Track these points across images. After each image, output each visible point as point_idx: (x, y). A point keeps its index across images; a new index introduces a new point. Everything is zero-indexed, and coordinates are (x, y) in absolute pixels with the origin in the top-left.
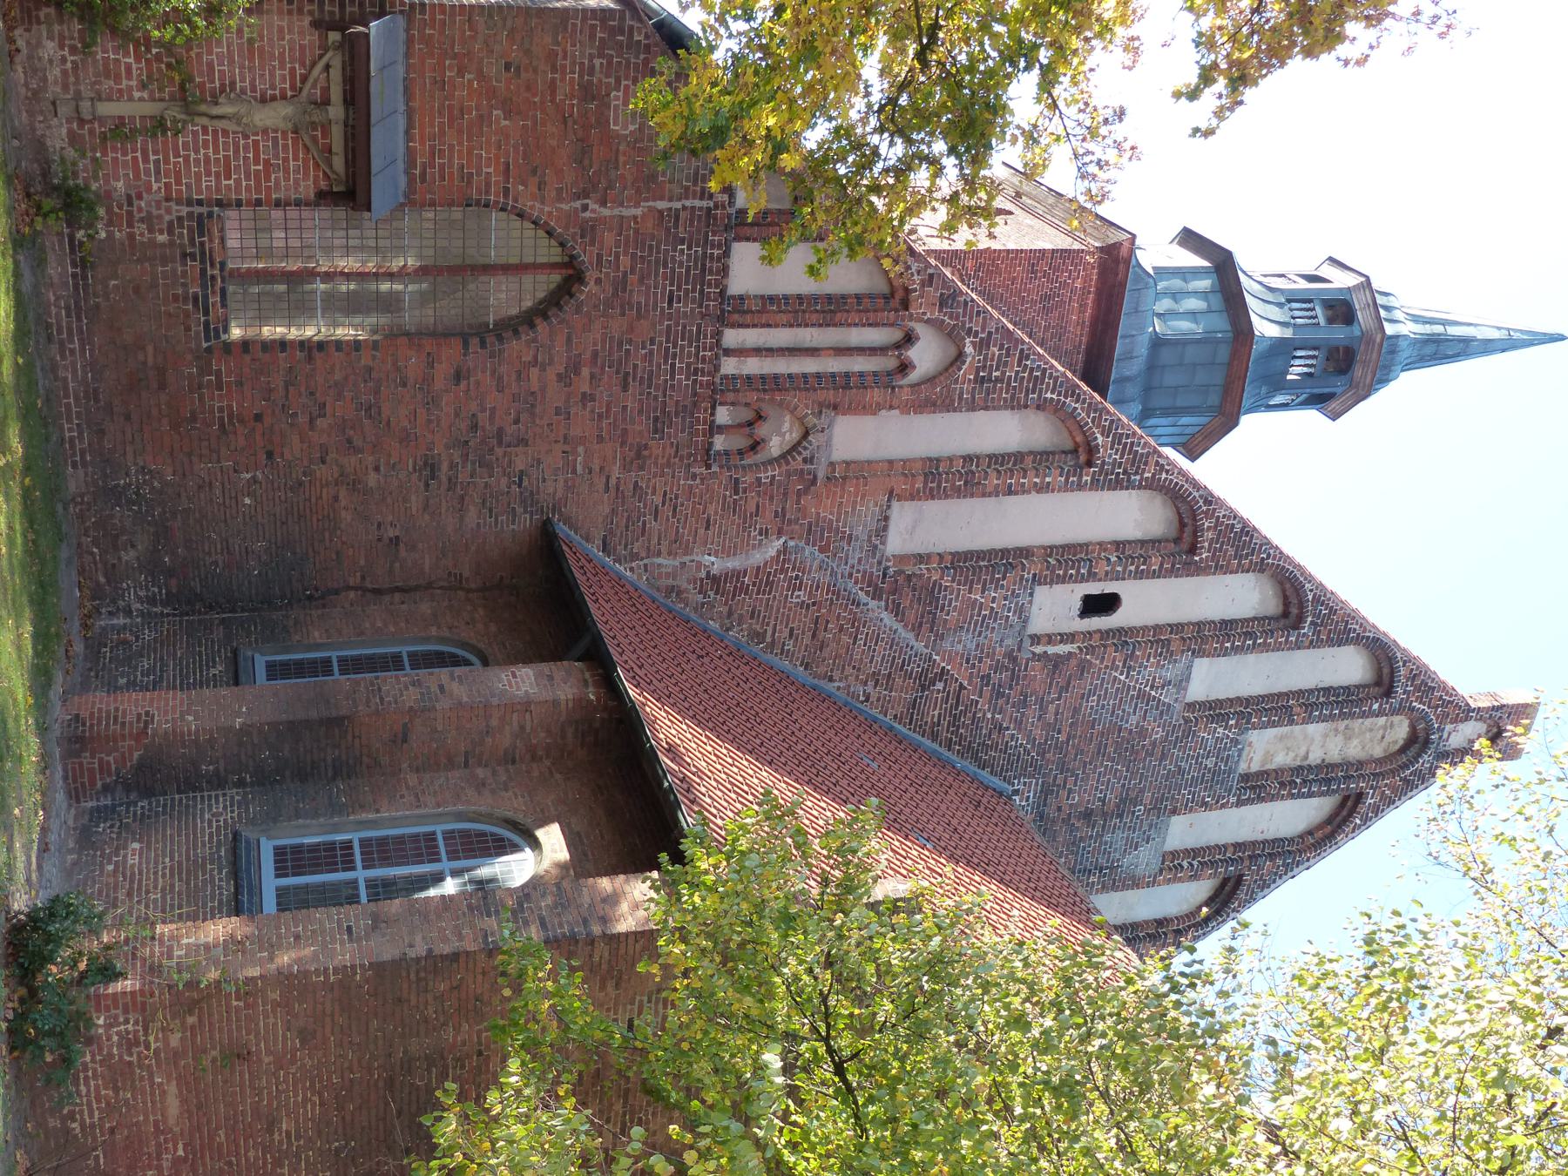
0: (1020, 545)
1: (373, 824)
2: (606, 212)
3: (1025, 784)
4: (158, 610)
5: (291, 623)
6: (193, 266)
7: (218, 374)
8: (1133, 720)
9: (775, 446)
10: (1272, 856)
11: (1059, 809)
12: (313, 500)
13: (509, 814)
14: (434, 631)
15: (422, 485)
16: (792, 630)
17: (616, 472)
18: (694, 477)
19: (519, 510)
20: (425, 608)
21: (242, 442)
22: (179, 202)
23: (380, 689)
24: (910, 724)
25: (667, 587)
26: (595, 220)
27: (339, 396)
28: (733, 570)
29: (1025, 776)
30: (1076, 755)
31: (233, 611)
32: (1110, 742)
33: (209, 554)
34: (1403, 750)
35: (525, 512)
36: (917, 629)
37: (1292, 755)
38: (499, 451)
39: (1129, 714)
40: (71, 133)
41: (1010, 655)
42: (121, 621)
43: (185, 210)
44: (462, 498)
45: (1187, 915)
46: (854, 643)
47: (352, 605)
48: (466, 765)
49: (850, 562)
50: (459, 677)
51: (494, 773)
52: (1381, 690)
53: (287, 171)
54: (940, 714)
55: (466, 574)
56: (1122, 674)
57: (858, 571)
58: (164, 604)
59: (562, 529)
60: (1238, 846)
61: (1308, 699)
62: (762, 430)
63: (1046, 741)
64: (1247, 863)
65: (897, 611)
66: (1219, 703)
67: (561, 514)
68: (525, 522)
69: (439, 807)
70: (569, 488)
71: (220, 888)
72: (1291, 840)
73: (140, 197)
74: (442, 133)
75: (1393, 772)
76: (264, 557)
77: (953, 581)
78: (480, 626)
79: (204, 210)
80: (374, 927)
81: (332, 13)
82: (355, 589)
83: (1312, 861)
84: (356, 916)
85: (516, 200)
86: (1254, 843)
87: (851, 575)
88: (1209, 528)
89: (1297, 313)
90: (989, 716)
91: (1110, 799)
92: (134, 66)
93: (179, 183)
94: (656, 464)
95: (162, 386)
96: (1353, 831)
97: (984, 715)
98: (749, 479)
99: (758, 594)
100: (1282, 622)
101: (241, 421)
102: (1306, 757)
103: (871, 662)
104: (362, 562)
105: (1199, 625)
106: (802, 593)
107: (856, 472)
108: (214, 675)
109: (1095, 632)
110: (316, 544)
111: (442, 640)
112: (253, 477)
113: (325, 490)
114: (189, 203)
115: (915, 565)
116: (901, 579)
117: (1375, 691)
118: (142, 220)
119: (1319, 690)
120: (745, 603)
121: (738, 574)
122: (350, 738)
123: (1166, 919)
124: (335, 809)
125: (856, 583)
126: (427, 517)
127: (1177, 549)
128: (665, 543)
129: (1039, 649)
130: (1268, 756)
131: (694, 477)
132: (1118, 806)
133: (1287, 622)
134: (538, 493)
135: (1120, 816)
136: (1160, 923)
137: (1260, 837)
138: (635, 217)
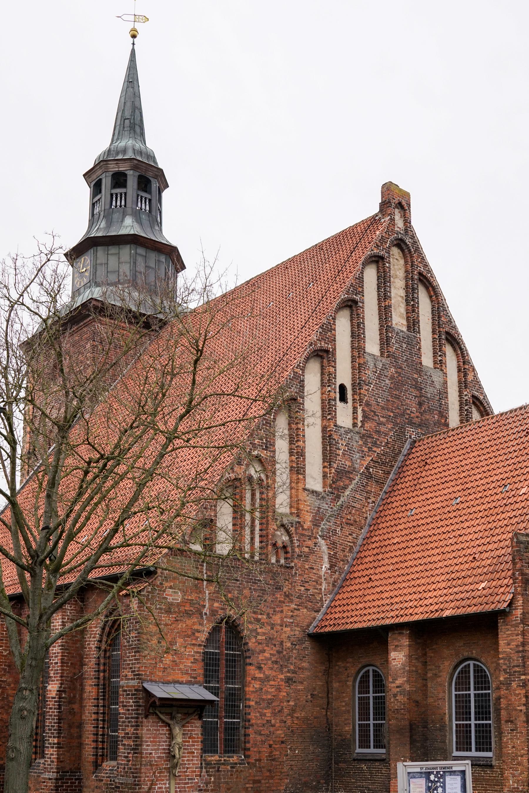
0: (321, 430)
2: (207, 605)
3: (408, 433)
4: (330, 788)
5: (339, 737)
6: (222, 768)
7: (256, 760)
8: (387, 382)
9: (285, 538)
10: (439, 317)
11: (417, 417)
12: (297, 726)
13: (452, 667)
14: (350, 683)
15: (294, 684)
16: (349, 534)
18: (296, 573)
19: (304, 646)
20: (336, 685)
21: (278, 753)
22: (201, 772)
23: (396, 709)
24: (383, 483)
25: (333, 586)
26: (210, 610)
28: (329, 559)
29: (405, 433)
30: (398, 408)
31: (332, 759)
32: (395, 393)
33: (313, 767)
34: (402, 250)
35: (304, 643)
36: (351, 479)
37: (401, 304)
38: (285, 653)
39: (385, 384)
41: (361, 438)
43: (204, 770)
44: (299, 668)
45: (457, 357)
46: (355, 507)
47: (332, 714)
48: (426, 680)
49: (327, 508)
50: (393, 680)
51: (431, 670)
52: (380, 261)
53: (192, 730)
54: (381, 470)
55: (324, 668)
56: (370, 386)
57: (330, 505)
58: (328, 786)
59: (311, 630)
60: (434, 332)
61: (382, 297)
62: (280, 544)
63: (392, 422)
64: (441, 329)
65: (345, 488)
66: (381, 339)
67: (306, 629)
69: (445, 692)
70: (297, 626)
71: (476, 771)
72: (433, 307)
73: (200, 786)
75: (412, 257)
76: (315, 746)
77: (335, 463)
78: (348, 665)
79: (203, 763)
80: (512, 722)
81: (142, 710)
82: (327, 712)
83: (443, 298)
84: (506, 727)
85: (203, 642)
86: (433, 324)
87: (332, 508)
88: (320, 344)
89: (118, 203)
90: (383, 448)
91: (415, 393)
92: (159, 786)
93: (195, 772)
94: (291, 589)
95: (259, 781)
96: (433, 277)
97: (382, 450)
98: (297, 550)
99: (337, 548)
102: (402, 297)
103: (362, 500)
104: (318, 709)
106: (338, 530)
108: (367, 768)
109: (353, 397)
110: (312, 726)
111: (451, 679)
112: (289, 749)
113: (295, 722)
114: (201, 768)
115: (328, 479)
116: (334, 486)
117: (381, 264)
118: (207, 786)
119: (378, 291)
120: (340, 554)
121: (330, 557)
122: (416, 722)
123: (458, 367)
124: (443, 728)
125: (334, 506)
126: (305, 683)
127: (326, 358)
130: (401, 316)
131: (296, 573)
132: (418, 390)
133: (354, 306)
134: (298, 638)
135: (421, 389)
136: (459, 371)
137: (431, 321)
138: (209, 594)
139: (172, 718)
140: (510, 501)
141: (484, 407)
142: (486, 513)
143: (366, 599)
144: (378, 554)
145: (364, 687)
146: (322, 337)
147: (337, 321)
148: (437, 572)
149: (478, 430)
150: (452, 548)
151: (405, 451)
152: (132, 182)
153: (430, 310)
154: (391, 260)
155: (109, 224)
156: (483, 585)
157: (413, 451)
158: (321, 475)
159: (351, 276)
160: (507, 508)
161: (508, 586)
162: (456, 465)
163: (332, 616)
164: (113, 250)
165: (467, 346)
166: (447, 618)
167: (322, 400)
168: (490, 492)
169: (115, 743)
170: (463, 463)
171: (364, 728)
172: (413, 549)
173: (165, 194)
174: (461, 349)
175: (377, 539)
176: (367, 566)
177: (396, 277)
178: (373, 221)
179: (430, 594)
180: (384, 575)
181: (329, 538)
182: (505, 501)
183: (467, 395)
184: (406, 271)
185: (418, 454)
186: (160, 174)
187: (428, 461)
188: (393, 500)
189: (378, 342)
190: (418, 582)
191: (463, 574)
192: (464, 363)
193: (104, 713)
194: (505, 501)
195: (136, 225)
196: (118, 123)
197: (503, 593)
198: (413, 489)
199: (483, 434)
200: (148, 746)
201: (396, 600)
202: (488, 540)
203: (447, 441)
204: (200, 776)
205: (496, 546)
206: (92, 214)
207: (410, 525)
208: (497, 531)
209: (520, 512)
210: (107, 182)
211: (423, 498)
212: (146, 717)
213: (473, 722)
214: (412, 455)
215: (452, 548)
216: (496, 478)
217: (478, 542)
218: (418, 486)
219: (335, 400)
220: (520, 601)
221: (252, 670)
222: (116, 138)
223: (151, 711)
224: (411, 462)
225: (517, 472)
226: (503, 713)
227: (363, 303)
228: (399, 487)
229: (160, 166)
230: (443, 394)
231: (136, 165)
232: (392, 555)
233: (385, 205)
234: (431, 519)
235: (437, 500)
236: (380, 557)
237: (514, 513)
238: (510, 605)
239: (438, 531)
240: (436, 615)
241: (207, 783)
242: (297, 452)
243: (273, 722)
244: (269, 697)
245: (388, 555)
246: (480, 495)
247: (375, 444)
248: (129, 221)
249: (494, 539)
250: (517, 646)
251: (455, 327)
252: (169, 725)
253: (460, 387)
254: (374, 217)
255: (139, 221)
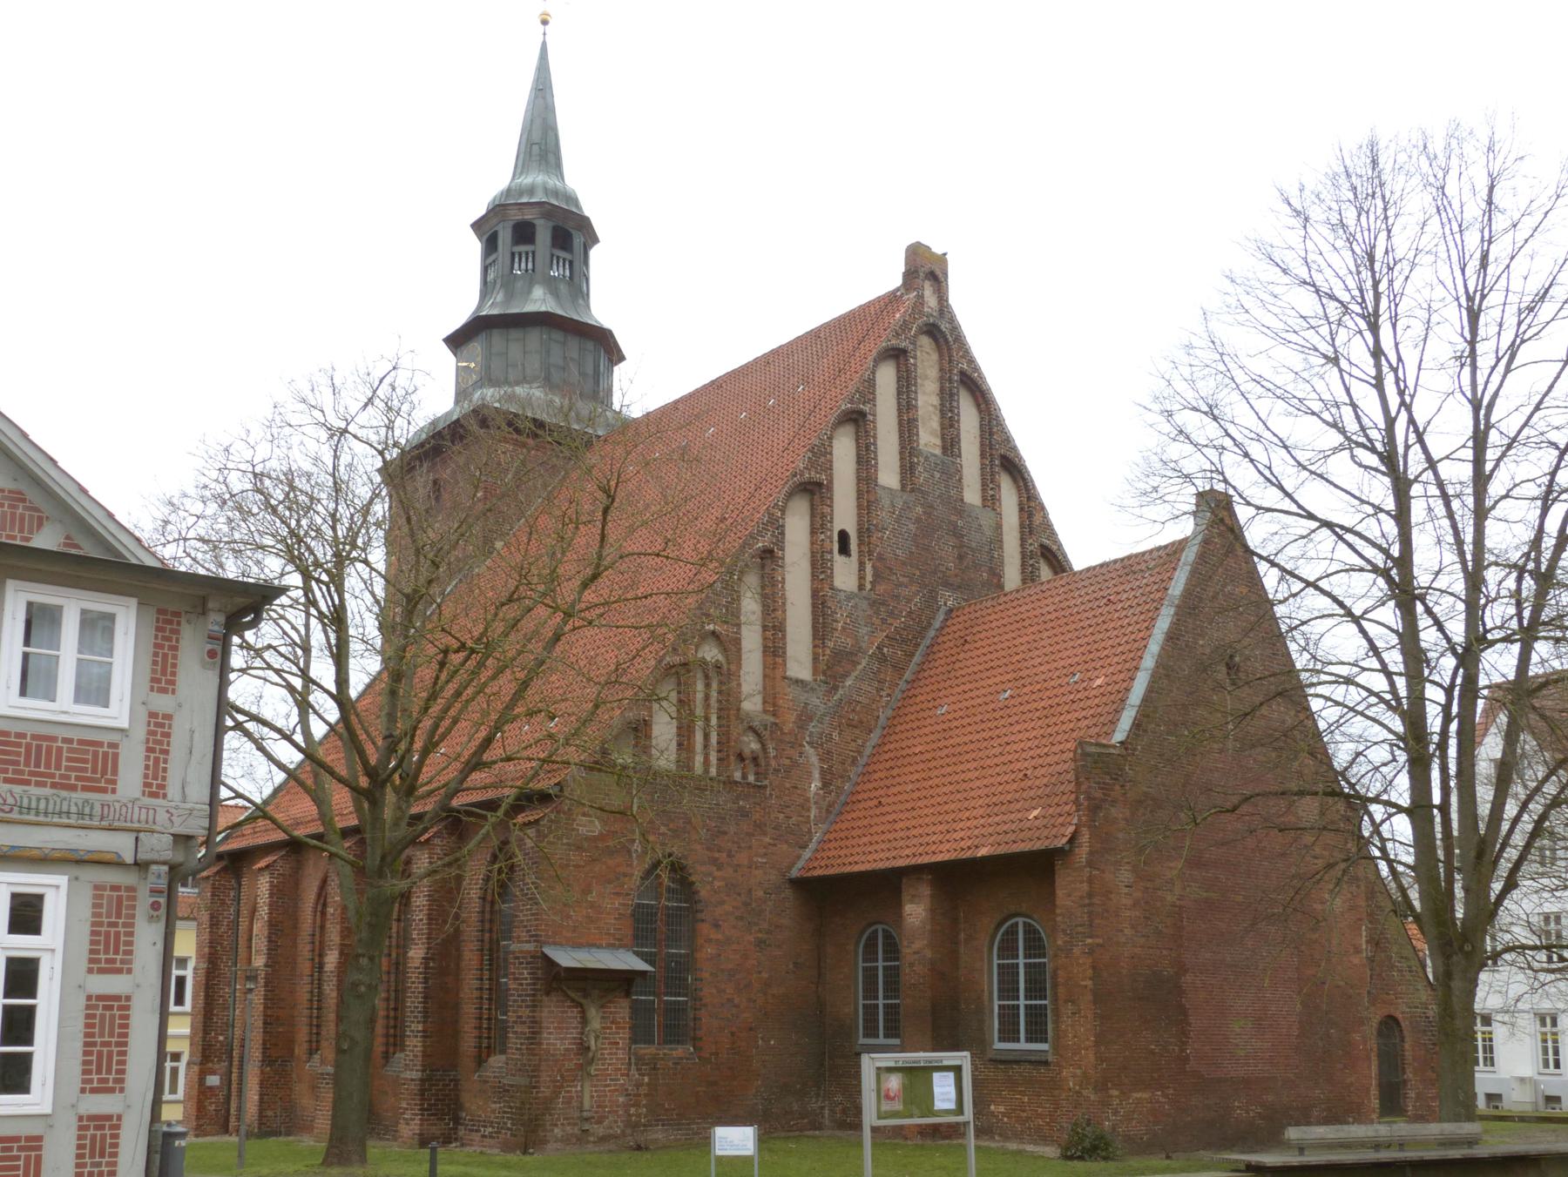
1: (991, 993)
7: (711, 1054)
8: (912, 526)
9: (755, 746)
10: (991, 434)
11: (956, 576)
13: (993, 926)
17: (767, 840)
27: (724, 991)
34: (936, 340)
37: (933, 417)
38: (754, 905)
40: (596, 1123)
42: (827, 1112)
44: (777, 927)
60: (983, 455)
62: (747, 752)
65: (845, 676)
66: (902, 466)
68: (788, 893)
72: (982, 419)
74: (598, 928)
75: (949, 349)
80: (1073, 1002)
98: (773, 763)
100: (861, 423)
101: (733, 1043)
105: (859, 480)
107: (771, 699)
111: (857, 944)
114: (630, 1064)
116: (829, 673)
117: (902, 359)
128: (804, 813)
129: (868, 586)
130: (933, 433)
135: (962, 536)
136: (1021, 510)
137: (978, 439)
139: (585, 997)
140: (1079, 696)
141: (1058, 561)
142: (1045, 712)
143: (872, 830)
144: (892, 768)
145: (1008, 948)
146: (812, 464)
147: (835, 442)
148: (972, 794)
149: (1041, 596)
150: (996, 761)
151: (937, 624)
152: (543, 236)
153: (978, 426)
154: (918, 354)
155: (510, 296)
156: (1035, 813)
157: (949, 623)
158: (810, 658)
159: (856, 377)
160: (1075, 706)
161: (1069, 815)
162: (1007, 644)
163: (824, 854)
164: (515, 334)
165: (1032, 474)
166: (983, 858)
167: (812, 552)
168: (1052, 683)
169: (504, 1028)
170: (1017, 642)
171: (871, 1011)
172: (942, 762)
173: (595, 253)
174: (1024, 479)
175: (892, 747)
176: (875, 785)
177: (926, 377)
178: (891, 299)
179: (961, 825)
180: (900, 797)
181: (822, 745)
182: (1072, 697)
183: (1033, 546)
184: (941, 370)
185: (954, 628)
186: (584, 225)
187: (968, 638)
188: (916, 692)
189: (898, 470)
190: (946, 807)
191: (1009, 797)
192: (1029, 498)
193: (490, 989)
194: (1072, 697)
195: (549, 298)
196: (523, 149)
197: (1062, 825)
198: (945, 678)
199: (1046, 602)
200: (550, 1033)
201: (915, 832)
202: (1046, 750)
203: (996, 610)
204: (628, 1075)
205: (1056, 758)
206: (485, 282)
207: (939, 728)
208: (1059, 738)
209: (1092, 712)
210: (505, 237)
211: (959, 690)
212: (548, 994)
213: (1022, 1002)
214: (947, 630)
215: (996, 761)
216: (1062, 663)
217: (1031, 753)
218: (953, 673)
219: (831, 552)
220: (1085, 837)
221: (705, 929)
222: (519, 171)
223: (554, 985)
224: (945, 639)
225: (1091, 656)
226: (1061, 990)
227: (874, 415)
228: (926, 674)
229: (587, 213)
230: (997, 541)
231: (548, 211)
232: (912, 769)
233: (910, 275)
234: (968, 720)
235: (977, 693)
236: (894, 772)
237: (1084, 713)
238: (1072, 840)
239: (978, 736)
240: (968, 854)
241: (638, 1085)
242: (774, 626)
243: (736, 1001)
244: (730, 966)
245: (906, 770)
246: (1038, 686)
247: (891, 614)
248: (538, 292)
249: (1054, 749)
250: (1082, 898)
251: (1014, 448)
252: (581, 1005)
253: (1022, 533)
254: (893, 293)
255: (555, 294)
